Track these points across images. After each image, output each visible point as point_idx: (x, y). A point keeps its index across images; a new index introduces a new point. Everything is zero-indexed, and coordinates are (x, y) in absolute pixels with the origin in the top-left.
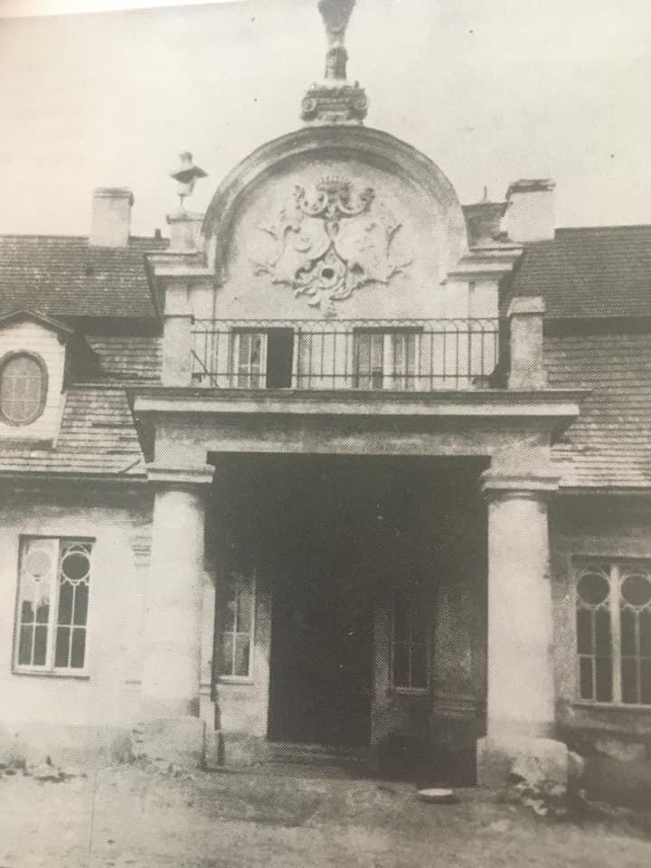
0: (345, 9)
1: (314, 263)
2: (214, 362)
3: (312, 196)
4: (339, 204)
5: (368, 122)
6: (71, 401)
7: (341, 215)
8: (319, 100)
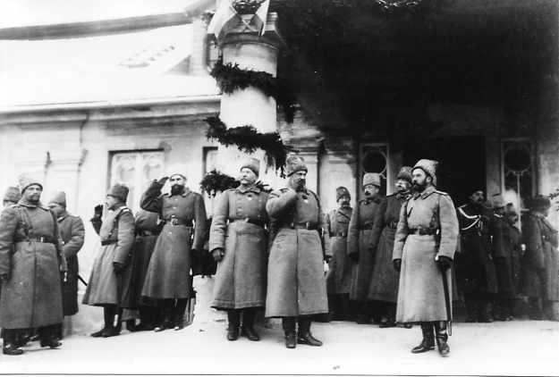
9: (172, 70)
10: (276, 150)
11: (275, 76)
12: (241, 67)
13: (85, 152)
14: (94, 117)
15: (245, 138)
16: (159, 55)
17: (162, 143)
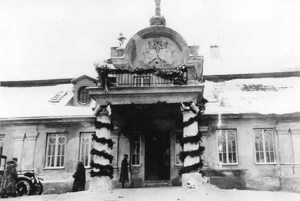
0: (167, 164)
1: (154, 60)
2: (139, 95)
3: (152, 44)
4: (159, 46)
5: (166, 26)
6: (193, 154)
7: (160, 48)
8: (153, 21)
9: (66, 105)
10: (110, 143)
11: (110, 123)
12: (102, 122)
13: (38, 134)
14: (42, 122)
15: (102, 141)
16: (62, 97)
17: (66, 131)
